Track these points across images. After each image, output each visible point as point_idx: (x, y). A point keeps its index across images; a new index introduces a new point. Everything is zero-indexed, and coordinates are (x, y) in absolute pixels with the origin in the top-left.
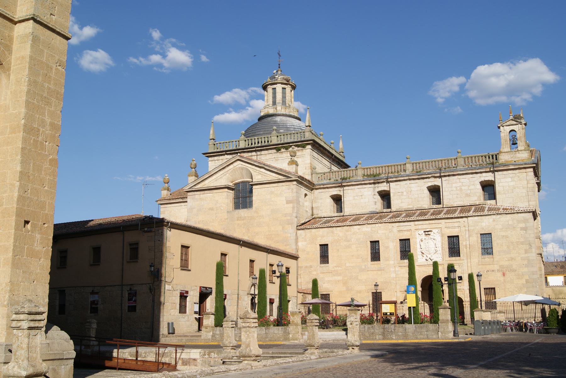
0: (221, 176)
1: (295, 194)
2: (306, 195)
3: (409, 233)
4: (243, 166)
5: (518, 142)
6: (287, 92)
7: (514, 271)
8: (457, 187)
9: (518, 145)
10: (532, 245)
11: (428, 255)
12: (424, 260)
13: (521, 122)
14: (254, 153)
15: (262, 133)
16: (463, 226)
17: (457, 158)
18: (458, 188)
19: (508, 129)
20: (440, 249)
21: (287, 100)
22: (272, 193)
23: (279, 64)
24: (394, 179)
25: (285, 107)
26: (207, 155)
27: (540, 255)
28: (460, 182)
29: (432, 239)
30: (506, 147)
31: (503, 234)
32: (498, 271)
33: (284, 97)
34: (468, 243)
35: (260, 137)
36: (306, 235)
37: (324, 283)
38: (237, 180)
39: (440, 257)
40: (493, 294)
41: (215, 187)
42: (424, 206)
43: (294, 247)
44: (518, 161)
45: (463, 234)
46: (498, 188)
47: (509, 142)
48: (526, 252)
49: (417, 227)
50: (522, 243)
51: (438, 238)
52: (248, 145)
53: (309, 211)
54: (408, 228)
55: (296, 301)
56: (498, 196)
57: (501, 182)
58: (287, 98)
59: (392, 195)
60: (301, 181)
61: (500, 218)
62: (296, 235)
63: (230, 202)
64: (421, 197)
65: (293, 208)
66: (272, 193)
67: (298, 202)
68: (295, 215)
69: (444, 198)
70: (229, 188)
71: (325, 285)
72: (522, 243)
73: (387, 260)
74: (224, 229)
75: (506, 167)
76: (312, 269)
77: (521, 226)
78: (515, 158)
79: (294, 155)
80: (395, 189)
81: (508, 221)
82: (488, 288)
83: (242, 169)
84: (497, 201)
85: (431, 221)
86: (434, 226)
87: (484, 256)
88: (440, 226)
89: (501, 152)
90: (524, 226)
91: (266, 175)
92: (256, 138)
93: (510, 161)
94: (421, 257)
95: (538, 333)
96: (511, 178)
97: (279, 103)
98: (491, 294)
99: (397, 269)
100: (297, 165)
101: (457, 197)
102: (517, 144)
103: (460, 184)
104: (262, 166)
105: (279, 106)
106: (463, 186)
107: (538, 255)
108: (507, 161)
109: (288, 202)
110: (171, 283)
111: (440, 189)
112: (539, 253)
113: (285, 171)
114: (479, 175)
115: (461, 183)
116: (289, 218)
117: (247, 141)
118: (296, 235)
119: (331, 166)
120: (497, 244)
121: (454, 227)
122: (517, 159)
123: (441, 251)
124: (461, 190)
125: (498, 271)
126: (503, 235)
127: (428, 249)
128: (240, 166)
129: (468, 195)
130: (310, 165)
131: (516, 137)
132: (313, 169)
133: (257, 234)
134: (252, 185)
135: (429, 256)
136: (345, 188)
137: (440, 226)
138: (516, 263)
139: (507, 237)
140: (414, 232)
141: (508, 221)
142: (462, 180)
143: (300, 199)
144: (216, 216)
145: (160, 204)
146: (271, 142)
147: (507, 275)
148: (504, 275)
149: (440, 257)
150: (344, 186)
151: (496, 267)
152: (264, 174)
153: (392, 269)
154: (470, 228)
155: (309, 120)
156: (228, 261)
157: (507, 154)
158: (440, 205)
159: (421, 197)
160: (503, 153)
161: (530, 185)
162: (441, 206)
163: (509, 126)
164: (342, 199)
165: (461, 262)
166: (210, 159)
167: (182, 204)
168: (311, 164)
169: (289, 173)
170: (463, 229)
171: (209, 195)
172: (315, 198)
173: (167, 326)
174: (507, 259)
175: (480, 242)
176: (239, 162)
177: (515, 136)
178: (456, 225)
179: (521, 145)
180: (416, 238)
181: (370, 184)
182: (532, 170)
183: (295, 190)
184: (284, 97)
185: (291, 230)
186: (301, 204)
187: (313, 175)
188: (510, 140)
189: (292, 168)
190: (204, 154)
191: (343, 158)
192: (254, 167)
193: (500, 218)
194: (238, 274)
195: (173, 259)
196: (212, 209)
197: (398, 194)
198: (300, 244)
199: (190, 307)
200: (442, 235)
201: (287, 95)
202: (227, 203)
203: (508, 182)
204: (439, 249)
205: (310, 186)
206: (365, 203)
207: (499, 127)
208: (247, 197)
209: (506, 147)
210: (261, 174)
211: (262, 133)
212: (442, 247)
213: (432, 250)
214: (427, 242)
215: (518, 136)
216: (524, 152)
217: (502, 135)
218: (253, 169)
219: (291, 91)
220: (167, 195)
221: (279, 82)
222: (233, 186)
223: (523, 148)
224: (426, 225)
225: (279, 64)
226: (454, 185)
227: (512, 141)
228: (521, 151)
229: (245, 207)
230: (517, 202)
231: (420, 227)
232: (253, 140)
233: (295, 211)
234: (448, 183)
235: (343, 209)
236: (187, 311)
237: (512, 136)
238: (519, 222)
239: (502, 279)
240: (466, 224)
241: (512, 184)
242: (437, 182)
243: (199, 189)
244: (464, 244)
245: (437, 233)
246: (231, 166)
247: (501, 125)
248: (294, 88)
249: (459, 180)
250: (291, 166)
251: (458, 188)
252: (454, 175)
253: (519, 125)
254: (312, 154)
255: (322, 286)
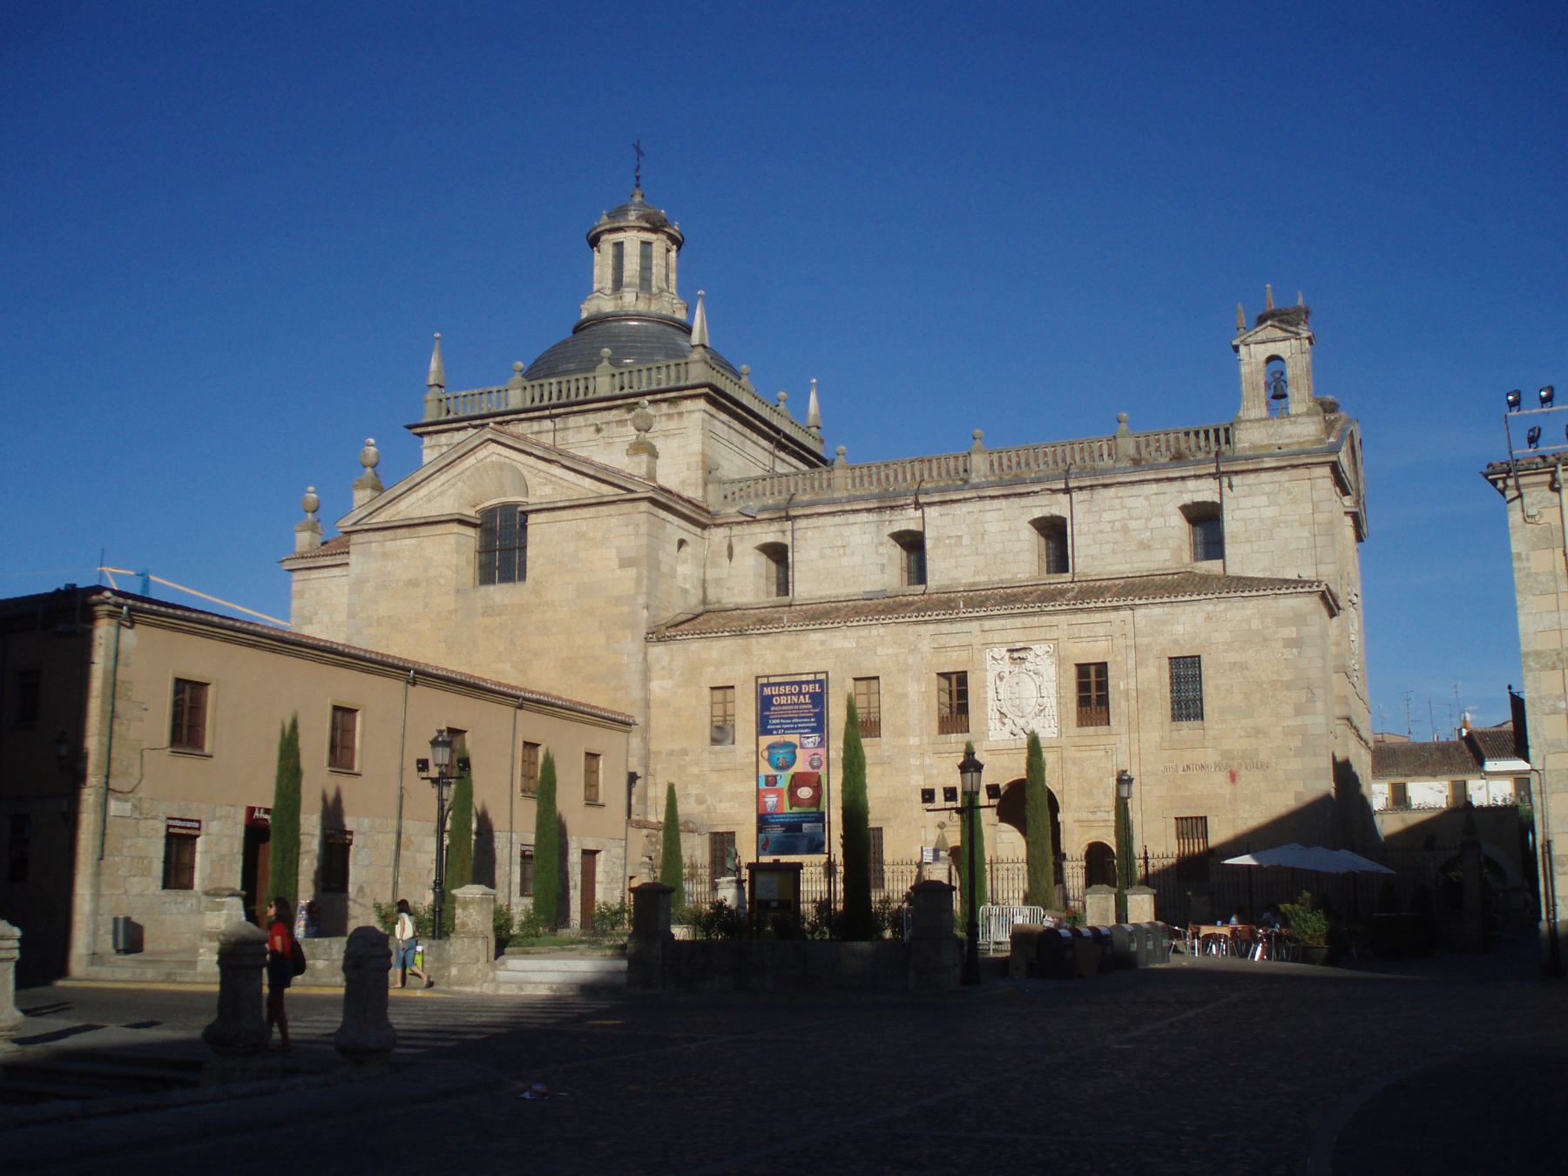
0: (440, 490)
1: (644, 541)
2: (682, 543)
3: (964, 655)
4: (503, 459)
5: (1290, 391)
6: (654, 254)
7: (1264, 767)
8: (1113, 522)
9: (1290, 399)
10: (1315, 691)
11: (1017, 720)
12: (1006, 734)
13: (1298, 334)
14: (547, 424)
15: (572, 366)
16: (1119, 634)
17: (1115, 438)
18: (1118, 525)
19: (1262, 352)
20: (1054, 701)
21: (654, 277)
22: (580, 536)
23: (638, 178)
24: (937, 499)
25: (648, 296)
26: (419, 430)
27: (1345, 722)
28: (1122, 508)
29: (1031, 673)
30: (1254, 406)
31: (1233, 657)
32: (1218, 766)
33: (646, 266)
34: (1132, 685)
35: (564, 379)
36: (672, 660)
37: (720, 801)
38: (488, 501)
39: (1052, 725)
40: (1200, 835)
41: (423, 521)
42: (1019, 576)
43: (637, 694)
44: (1287, 445)
45: (1119, 659)
46: (1231, 524)
47: (1262, 391)
48: (1299, 710)
49: (990, 637)
50: (1288, 686)
51: (1049, 670)
52: (533, 400)
53: (692, 591)
54: (964, 639)
55: (621, 851)
56: (1229, 549)
57: (1238, 508)
58: (654, 270)
59: (929, 544)
60: (664, 501)
61: (1225, 610)
62: (645, 658)
63: (464, 564)
64: (1012, 551)
65: (638, 580)
66: (580, 536)
67: (653, 563)
68: (642, 600)
69: (1076, 555)
70: (461, 522)
71: (722, 805)
72: (1288, 686)
73: (901, 732)
74: (445, 641)
75: (1254, 464)
76: (687, 758)
77: (1286, 636)
78: (1280, 437)
79: (646, 427)
80: (937, 524)
81: (1248, 621)
82: (1186, 818)
83: (501, 466)
84: (1227, 563)
85: (1030, 619)
86: (1037, 633)
87: (1179, 723)
88: (1055, 634)
89: (1240, 421)
90: (1294, 635)
91: (565, 484)
92: (553, 380)
93: (1265, 447)
94: (999, 725)
95: (1278, 960)
96: (1268, 495)
97: (629, 285)
98: (1195, 835)
99: (928, 761)
100: (654, 454)
101: (1114, 552)
102: (1285, 396)
103: (1124, 513)
104: (554, 458)
105: (628, 292)
106: (1132, 519)
107: (1338, 722)
108: (1255, 447)
109: (625, 563)
110: (131, 795)
111: (1065, 526)
112: (1345, 713)
113: (616, 472)
114: (1177, 484)
115: (1126, 510)
116: (626, 609)
117: (529, 389)
118: (645, 658)
119: (774, 462)
120: (1217, 687)
121: (1095, 638)
122: (1286, 441)
123: (1055, 708)
124: (1125, 529)
125: (1218, 766)
126: (1233, 661)
127: (1017, 702)
128: (494, 458)
129: (1144, 546)
130: (700, 459)
131: (1282, 378)
132: (709, 470)
133: (535, 655)
134: (525, 514)
135: (1021, 722)
136: (801, 523)
137: (1055, 634)
138: (1269, 746)
139: (1243, 667)
140: (979, 650)
141: (1248, 621)
142: (1130, 502)
143: (662, 556)
144: (425, 606)
145: (289, 570)
146: (594, 392)
147: (1244, 780)
148: (1233, 777)
149: (1052, 725)
150: (795, 517)
151: (1211, 756)
152: (561, 482)
153: (914, 762)
154: (1139, 640)
155: (702, 327)
156: (363, 735)
157: (1256, 425)
158: (1064, 575)
159: (1012, 551)
160: (1246, 421)
161: (1320, 517)
162: (1067, 577)
163: (1264, 342)
164: (790, 555)
165: (1113, 739)
166: (426, 440)
167: (336, 571)
168: (703, 454)
169: (630, 477)
170: (1120, 642)
171: (408, 542)
172: (713, 552)
173: (110, 927)
174: (1243, 734)
175: (1168, 680)
176: (493, 447)
177: (1282, 374)
178: (1100, 630)
179: (1299, 399)
180: (986, 670)
181: (869, 510)
182: (1326, 471)
183: (644, 529)
184: (646, 266)
185: (630, 645)
186: (664, 568)
187: (710, 487)
188: (1267, 385)
189: (639, 464)
190: (410, 427)
191: (818, 444)
192: (532, 461)
193: (1225, 610)
194: (402, 770)
195: (141, 719)
196: (413, 583)
197: (947, 542)
198: (655, 686)
199: (208, 871)
200: (1060, 662)
201: (654, 262)
202: (456, 566)
203: (1259, 507)
204: (1051, 702)
205: (699, 517)
206: (854, 567)
207: (1236, 348)
208: (514, 549)
209: (1254, 406)
210: (551, 481)
211: (572, 366)
212: (1060, 698)
213: (1030, 706)
214: (1016, 680)
215: (1289, 373)
216: (1306, 419)
217: (1244, 370)
218: (530, 469)
219: (668, 251)
220: (311, 545)
221: (632, 224)
222: (478, 516)
223: (1302, 409)
224: (1010, 629)
225: (638, 178)
226: (1107, 516)
227: (1272, 387)
228: (1298, 415)
229: (490, 580)
230: (1283, 567)
231: (996, 637)
232: (546, 388)
233: (644, 589)
234: (1089, 511)
235: (790, 585)
236: (197, 881)
237: (1273, 375)
238: (1280, 622)
239: (1227, 790)
240: (1129, 628)
241: (1268, 513)
242: (1057, 506)
243: (380, 526)
244: (1122, 687)
245: (1046, 656)
246: (471, 461)
247: (1242, 342)
248: (678, 242)
249: (1118, 501)
250: (636, 459)
251: (1117, 523)
252: (1105, 486)
253: (1292, 341)
254: (707, 426)
255: (715, 808)
